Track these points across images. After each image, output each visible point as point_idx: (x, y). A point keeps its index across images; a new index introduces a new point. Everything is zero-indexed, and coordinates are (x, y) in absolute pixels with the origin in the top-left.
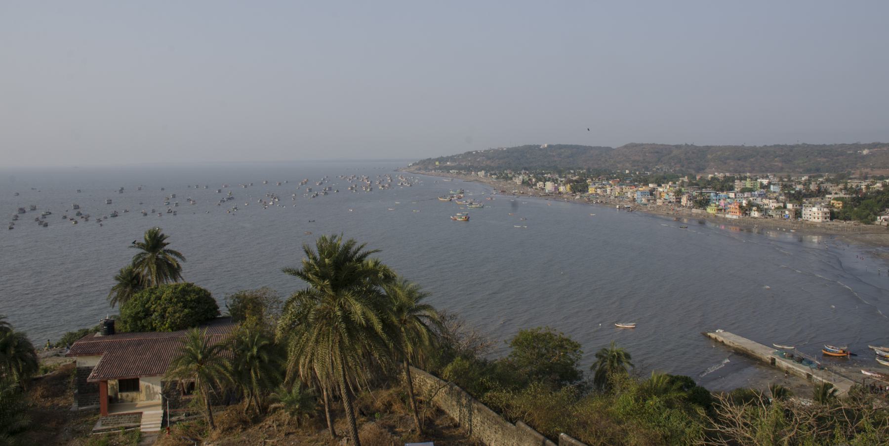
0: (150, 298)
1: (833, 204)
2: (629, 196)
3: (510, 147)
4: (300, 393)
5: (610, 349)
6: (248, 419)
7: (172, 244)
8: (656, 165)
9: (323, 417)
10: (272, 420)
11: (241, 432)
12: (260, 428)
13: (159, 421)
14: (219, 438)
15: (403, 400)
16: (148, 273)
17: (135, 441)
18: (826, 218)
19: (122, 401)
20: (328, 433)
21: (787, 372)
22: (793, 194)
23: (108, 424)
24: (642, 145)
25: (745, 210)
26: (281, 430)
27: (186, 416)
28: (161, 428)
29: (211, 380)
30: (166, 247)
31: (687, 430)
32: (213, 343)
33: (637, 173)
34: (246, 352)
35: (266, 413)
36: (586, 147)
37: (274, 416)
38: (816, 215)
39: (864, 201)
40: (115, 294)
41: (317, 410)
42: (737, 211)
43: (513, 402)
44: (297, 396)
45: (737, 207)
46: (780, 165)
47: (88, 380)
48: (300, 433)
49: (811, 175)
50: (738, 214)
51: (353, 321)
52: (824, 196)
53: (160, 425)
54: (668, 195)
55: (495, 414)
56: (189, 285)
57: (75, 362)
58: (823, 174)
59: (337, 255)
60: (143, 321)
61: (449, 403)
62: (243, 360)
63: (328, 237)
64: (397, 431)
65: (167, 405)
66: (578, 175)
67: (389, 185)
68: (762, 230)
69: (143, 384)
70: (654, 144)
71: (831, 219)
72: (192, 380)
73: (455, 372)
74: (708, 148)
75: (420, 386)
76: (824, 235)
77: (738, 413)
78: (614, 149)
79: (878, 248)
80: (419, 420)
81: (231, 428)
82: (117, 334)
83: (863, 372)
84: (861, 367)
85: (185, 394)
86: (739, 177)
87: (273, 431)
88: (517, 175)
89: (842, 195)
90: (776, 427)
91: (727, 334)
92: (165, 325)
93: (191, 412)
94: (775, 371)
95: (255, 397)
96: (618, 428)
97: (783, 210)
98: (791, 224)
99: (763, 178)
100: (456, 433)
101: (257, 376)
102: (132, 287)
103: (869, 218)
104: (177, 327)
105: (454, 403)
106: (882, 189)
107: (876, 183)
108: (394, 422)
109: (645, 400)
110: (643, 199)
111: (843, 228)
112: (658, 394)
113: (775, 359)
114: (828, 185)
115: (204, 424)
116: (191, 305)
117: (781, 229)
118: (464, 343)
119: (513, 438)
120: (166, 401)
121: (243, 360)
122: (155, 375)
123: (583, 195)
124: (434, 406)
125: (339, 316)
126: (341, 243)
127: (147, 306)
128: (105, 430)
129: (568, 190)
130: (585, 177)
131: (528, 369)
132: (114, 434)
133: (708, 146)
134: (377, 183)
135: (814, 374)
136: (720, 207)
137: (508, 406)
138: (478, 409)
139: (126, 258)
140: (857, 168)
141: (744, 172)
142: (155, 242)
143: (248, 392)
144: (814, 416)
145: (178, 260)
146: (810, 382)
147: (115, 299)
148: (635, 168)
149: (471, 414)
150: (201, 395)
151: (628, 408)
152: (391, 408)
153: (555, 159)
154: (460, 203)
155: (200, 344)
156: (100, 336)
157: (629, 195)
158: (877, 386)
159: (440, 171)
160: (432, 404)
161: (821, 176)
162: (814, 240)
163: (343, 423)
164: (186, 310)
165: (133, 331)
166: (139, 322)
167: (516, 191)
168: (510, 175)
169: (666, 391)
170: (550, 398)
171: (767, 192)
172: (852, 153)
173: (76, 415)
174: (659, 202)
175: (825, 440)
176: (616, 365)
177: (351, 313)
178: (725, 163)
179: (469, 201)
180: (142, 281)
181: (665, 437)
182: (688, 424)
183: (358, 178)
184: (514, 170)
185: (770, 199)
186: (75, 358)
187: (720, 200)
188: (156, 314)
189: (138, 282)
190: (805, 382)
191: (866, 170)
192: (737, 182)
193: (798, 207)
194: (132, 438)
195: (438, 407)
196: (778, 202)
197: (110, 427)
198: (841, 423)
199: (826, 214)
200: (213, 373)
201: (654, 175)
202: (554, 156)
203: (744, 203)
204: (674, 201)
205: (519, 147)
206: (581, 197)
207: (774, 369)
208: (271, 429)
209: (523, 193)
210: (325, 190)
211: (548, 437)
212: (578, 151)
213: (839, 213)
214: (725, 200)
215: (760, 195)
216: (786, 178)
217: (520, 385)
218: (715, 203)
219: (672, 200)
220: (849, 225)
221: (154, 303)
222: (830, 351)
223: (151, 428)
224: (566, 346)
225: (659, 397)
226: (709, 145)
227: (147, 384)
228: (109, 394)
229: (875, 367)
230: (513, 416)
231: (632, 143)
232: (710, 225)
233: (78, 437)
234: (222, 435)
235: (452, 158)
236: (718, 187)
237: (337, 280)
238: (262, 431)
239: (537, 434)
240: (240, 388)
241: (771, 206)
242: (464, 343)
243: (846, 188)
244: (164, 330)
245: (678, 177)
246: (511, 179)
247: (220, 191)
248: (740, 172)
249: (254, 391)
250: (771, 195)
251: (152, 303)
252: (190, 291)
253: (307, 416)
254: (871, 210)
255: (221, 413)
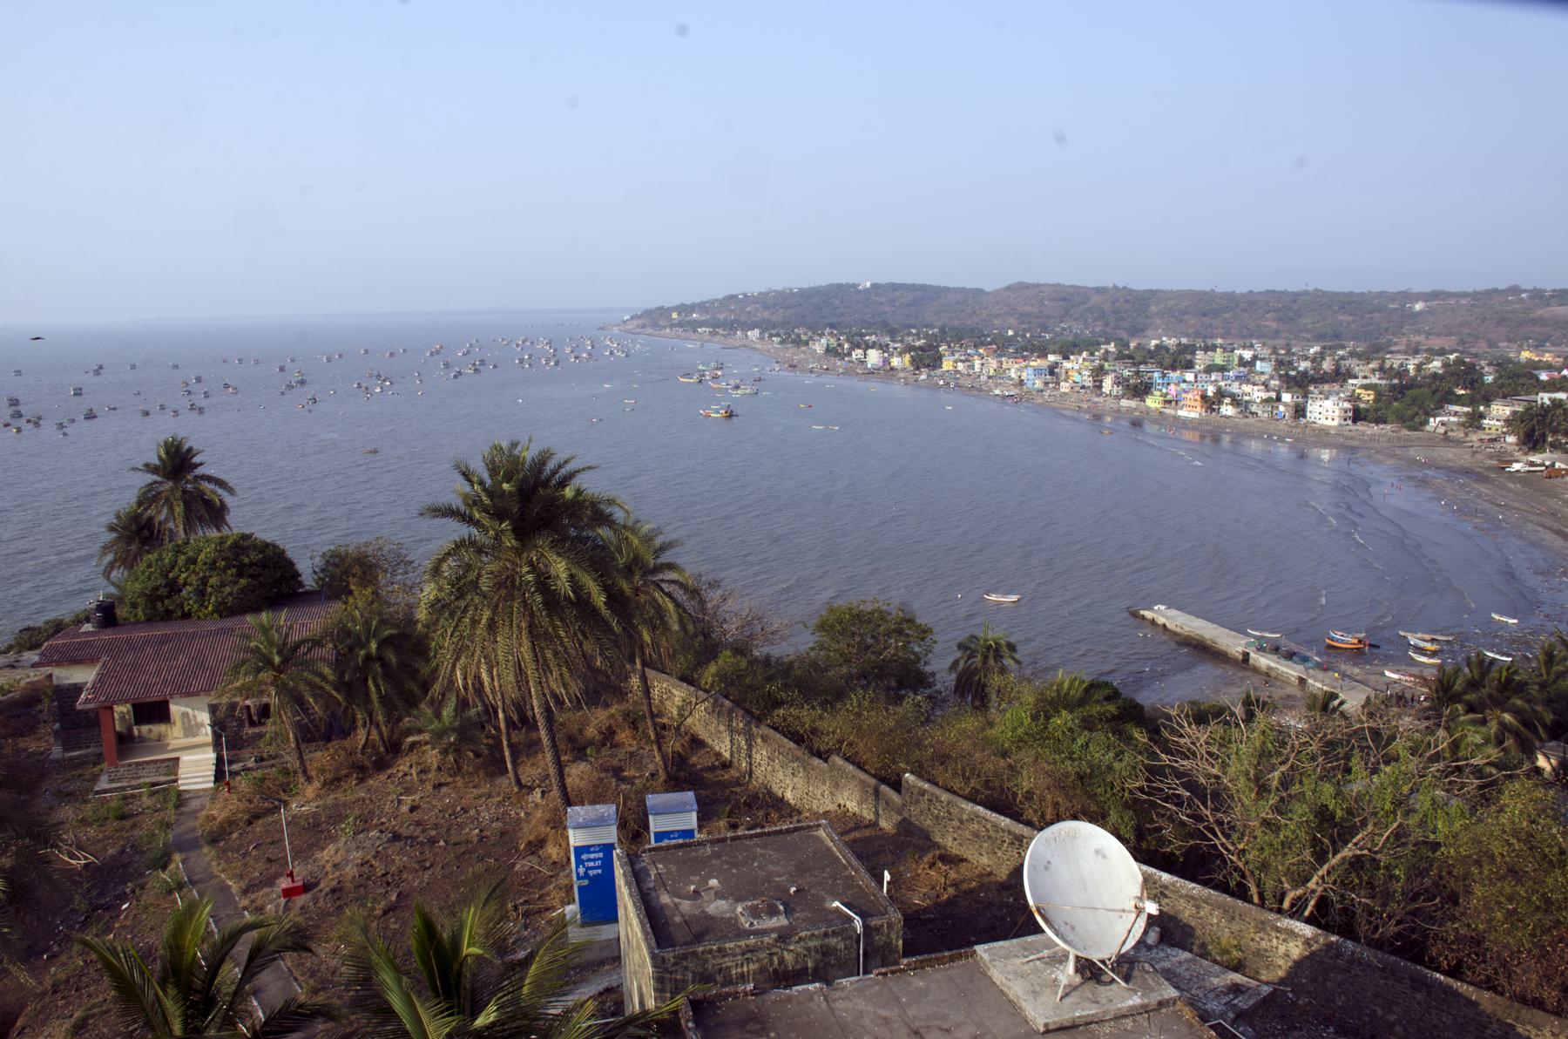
0: (176, 561)
1: (1359, 394)
2: (1013, 375)
3: (804, 287)
4: (456, 716)
5: (982, 635)
6: (367, 763)
7: (210, 463)
8: (1062, 322)
9: (498, 756)
10: (408, 764)
11: (357, 785)
12: (389, 777)
13: (210, 771)
14: (318, 796)
15: (634, 725)
16: (170, 519)
17: (170, 805)
18: (1345, 420)
19: (142, 739)
20: (507, 781)
21: (1268, 675)
22: (1294, 378)
23: (119, 780)
24: (1038, 285)
25: (1210, 403)
26: (425, 781)
27: (256, 761)
28: (215, 782)
29: (300, 701)
30: (199, 471)
31: (1117, 765)
32: (295, 637)
33: (1028, 335)
34: (357, 650)
35: (397, 752)
36: (938, 287)
37: (414, 758)
38: (1330, 413)
39: (1411, 391)
40: (110, 557)
41: (485, 745)
42: (1198, 404)
43: (822, 725)
44: (450, 722)
45: (1198, 398)
46: (1274, 325)
47: (79, 706)
48: (459, 784)
49: (1327, 344)
50: (1199, 409)
51: (555, 590)
52: (1345, 381)
53: (213, 779)
54: (1080, 374)
55: (792, 745)
56: (245, 537)
57: (50, 676)
58: (1345, 343)
59: (521, 476)
60: (166, 602)
61: (712, 728)
62: (352, 663)
63: (505, 444)
64: (626, 776)
65: (222, 744)
66: (925, 338)
67: (590, 354)
68: (1240, 435)
69: (175, 709)
70: (1058, 285)
71: (1355, 420)
72: (265, 700)
73: (723, 676)
74: (1153, 293)
75: (661, 701)
76: (1341, 447)
77: (1197, 736)
78: (987, 293)
79: (1427, 472)
80: (664, 757)
81: (338, 779)
82: (122, 625)
83: (1387, 673)
84: (1385, 665)
85: (252, 724)
86: (1203, 345)
87: (412, 781)
88: (817, 338)
89: (1374, 380)
90: (1260, 757)
91: (1173, 612)
92: (207, 608)
93: (265, 755)
94: (1248, 673)
95: (378, 726)
96: (1002, 763)
97: (1276, 405)
98: (1286, 428)
99: (1244, 347)
100: (726, 777)
101: (380, 690)
102: (140, 543)
103: (1416, 420)
104: (228, 610)
105: (722, 728)
106: (1440, 372)
107: (1433, 360)
108: (620, 760)
109: (1048, 718)
110: (1037, 381)
111: (1372, 438)
112: (1070, 707)
113: (1248, 654)
114: (1352, 363)
115: (289, 774)
116: (251, 571)
117: (1270, 436)
118: (732, 629)
119: (824, 783)
120: (221, 737)
121: (352, 663)
122: (196, 694)
123: (932, 373)
124: (686, 734)
125: (529, 582)
126: (529, 455)
127: (171, 575)
128: (115, 790)
129: (907, 364)
130: (936, 341)
131: (844, 670)
132: (133, 796)
133: (1152, 290)
134: (568, 350)
135: (1309, 677)
136: (1169, 397)
137: (814, 731)
138: (762, 737)
139: (125, 491)
140: (1404, 334)
141: (1213, 337)
142: (177, 461)
143: (364, 719)
144: (1321, 739)
145: (220, 491)
146: (1303, 690)
147: (111, 566)
148: (1025, 326)
149: (750, 746)
150: (281, 725)
151: (1020, 731)
152: (613, 739)
153: (885, 309)
154: (716, 386)
155: (276, 638)
156: (91, 629)
157: (1013, 374)
158: (1408, 696)
159: (681, 330)
160: (682, 730)
161: (1343, 347)
162: (1323, 457)
163: (533, 765)
164: (243, 581)
165: (149, 620)
166: (159, 605)
167: (814, 365)
168: (804, 338)
169: (1082, 702)
170: (883, 717)
171: (1250, 372)
172: (1396, 309)
173: (61, 765)
174: (1065, 387)
175: (1335, 776)
176: (991, 662)
177: (549, 577)
178: (1182, 321)
179: (732, 382)
180: (159, 531)
181: (1081, 777)
182: (1119, 755)
183: (532, 343)
184: (810, 328)
185: (1254, 384)
186: (47, 670)
187: (1168, 384)
188: (189, 588)
189: (152, 533)
190: (1294, 691)
191: (1417, 338)
192: (1200, 354)
193: (1300, 400)
194: (165, 801)
195: (692, 735)
196: (1268, 391)
197: (125, 784)
198: (1362, 749)
199: (1346, 412)
200: (302, 687)
201: (1057, 339)
202: (882, 304)
203: (1211, 390)
204: (1091, 385)
205: (820, 287)
206: (928, 376)
207: (1246, 669)
208: (408, 778)
209: (827, 369)
210: (474, 365)
211: (883, 780)
212: (924, 295)
213: (1367, 410)
214: (1177, 384)
215: (1237, 378)
216: (1283, 349)
217: (833, 697)
218: (1161, 390)
219: (1087, 384)
220: (1383, 432)
221: (183, 570)
222: (1337, 641)
223: (196, 783)
224: (907, 632)
225: (1071, 712)
226: (1154, 288)
227: (183, 709)
228: (118, 728)
229: (1407, 666)
230: (823, 748)
231: (1020, 283)
232: (1151, 428)
233: (69, 802)
234: (323, 792)
235: (701, 307)
236: (1168, 361)
237: (523, 520)
238: (393, 783)
239: (864, 776)
240: (350, 710)
241: (1255, 396)
242: (732, 629)
243: (1381, 369)
244: (206, 616)
245: (1099, 344)
246: (807, 343)
247: (282, 369)
248: (1205, 337)
249: (374, 714)
250: (1257, 378)
251: (180, 570)
252: (248, 548)
253: (471, 755)
254: (1421, 406)
255: (319, 754)
